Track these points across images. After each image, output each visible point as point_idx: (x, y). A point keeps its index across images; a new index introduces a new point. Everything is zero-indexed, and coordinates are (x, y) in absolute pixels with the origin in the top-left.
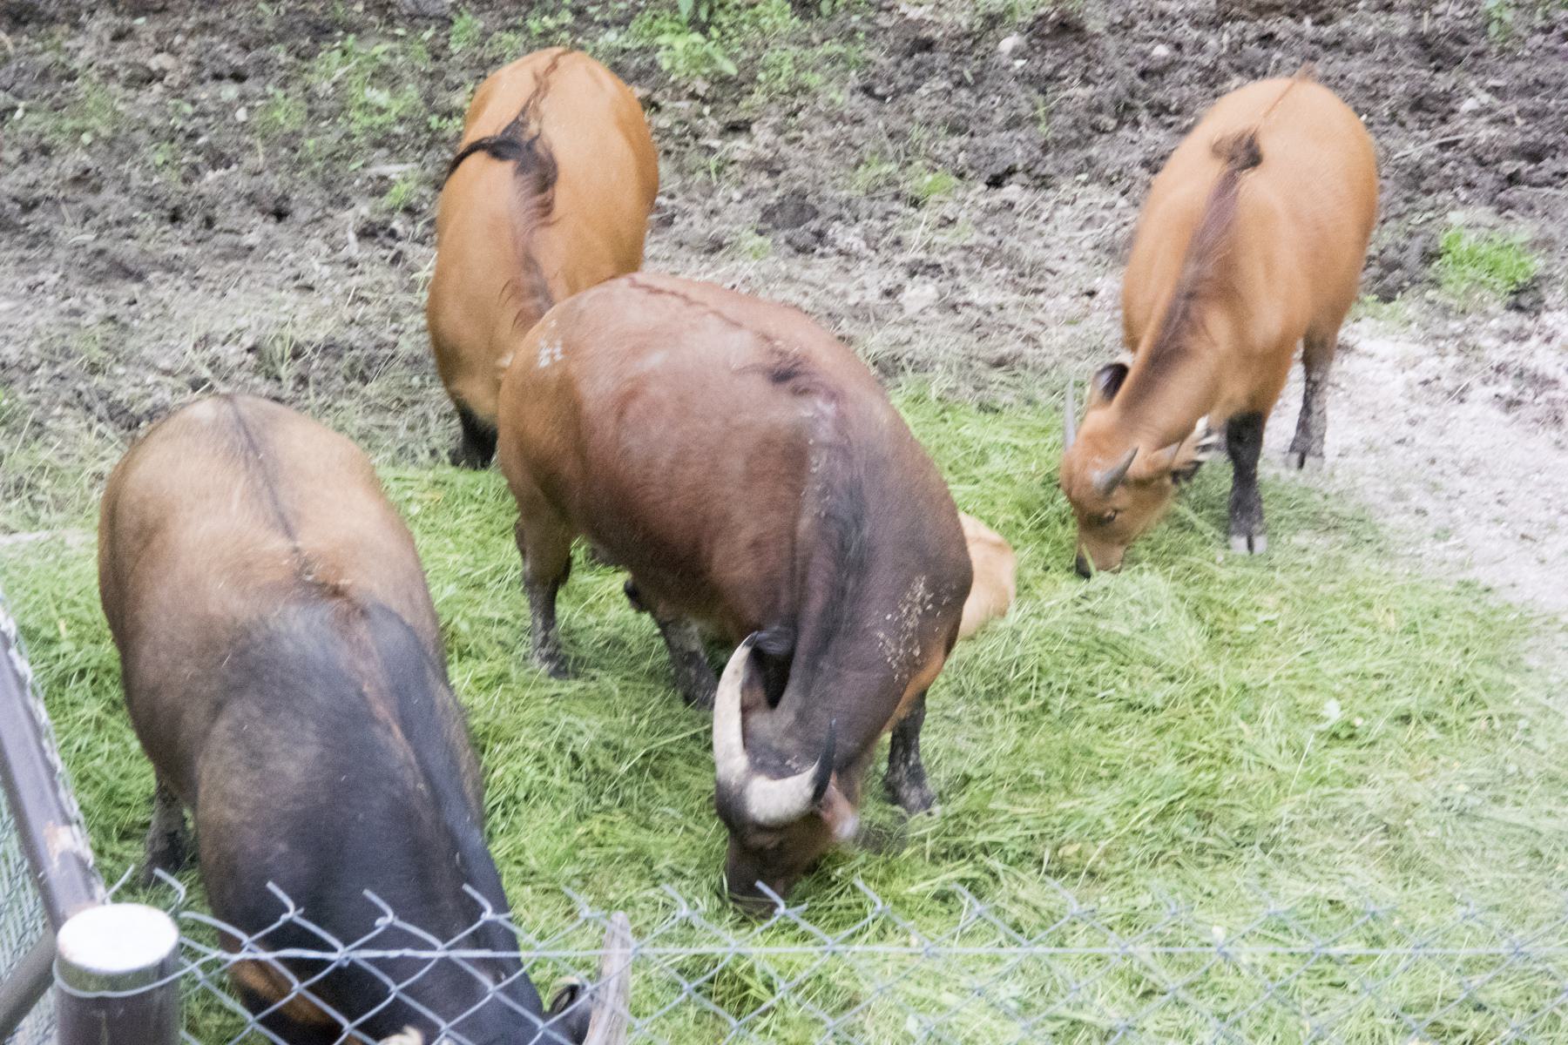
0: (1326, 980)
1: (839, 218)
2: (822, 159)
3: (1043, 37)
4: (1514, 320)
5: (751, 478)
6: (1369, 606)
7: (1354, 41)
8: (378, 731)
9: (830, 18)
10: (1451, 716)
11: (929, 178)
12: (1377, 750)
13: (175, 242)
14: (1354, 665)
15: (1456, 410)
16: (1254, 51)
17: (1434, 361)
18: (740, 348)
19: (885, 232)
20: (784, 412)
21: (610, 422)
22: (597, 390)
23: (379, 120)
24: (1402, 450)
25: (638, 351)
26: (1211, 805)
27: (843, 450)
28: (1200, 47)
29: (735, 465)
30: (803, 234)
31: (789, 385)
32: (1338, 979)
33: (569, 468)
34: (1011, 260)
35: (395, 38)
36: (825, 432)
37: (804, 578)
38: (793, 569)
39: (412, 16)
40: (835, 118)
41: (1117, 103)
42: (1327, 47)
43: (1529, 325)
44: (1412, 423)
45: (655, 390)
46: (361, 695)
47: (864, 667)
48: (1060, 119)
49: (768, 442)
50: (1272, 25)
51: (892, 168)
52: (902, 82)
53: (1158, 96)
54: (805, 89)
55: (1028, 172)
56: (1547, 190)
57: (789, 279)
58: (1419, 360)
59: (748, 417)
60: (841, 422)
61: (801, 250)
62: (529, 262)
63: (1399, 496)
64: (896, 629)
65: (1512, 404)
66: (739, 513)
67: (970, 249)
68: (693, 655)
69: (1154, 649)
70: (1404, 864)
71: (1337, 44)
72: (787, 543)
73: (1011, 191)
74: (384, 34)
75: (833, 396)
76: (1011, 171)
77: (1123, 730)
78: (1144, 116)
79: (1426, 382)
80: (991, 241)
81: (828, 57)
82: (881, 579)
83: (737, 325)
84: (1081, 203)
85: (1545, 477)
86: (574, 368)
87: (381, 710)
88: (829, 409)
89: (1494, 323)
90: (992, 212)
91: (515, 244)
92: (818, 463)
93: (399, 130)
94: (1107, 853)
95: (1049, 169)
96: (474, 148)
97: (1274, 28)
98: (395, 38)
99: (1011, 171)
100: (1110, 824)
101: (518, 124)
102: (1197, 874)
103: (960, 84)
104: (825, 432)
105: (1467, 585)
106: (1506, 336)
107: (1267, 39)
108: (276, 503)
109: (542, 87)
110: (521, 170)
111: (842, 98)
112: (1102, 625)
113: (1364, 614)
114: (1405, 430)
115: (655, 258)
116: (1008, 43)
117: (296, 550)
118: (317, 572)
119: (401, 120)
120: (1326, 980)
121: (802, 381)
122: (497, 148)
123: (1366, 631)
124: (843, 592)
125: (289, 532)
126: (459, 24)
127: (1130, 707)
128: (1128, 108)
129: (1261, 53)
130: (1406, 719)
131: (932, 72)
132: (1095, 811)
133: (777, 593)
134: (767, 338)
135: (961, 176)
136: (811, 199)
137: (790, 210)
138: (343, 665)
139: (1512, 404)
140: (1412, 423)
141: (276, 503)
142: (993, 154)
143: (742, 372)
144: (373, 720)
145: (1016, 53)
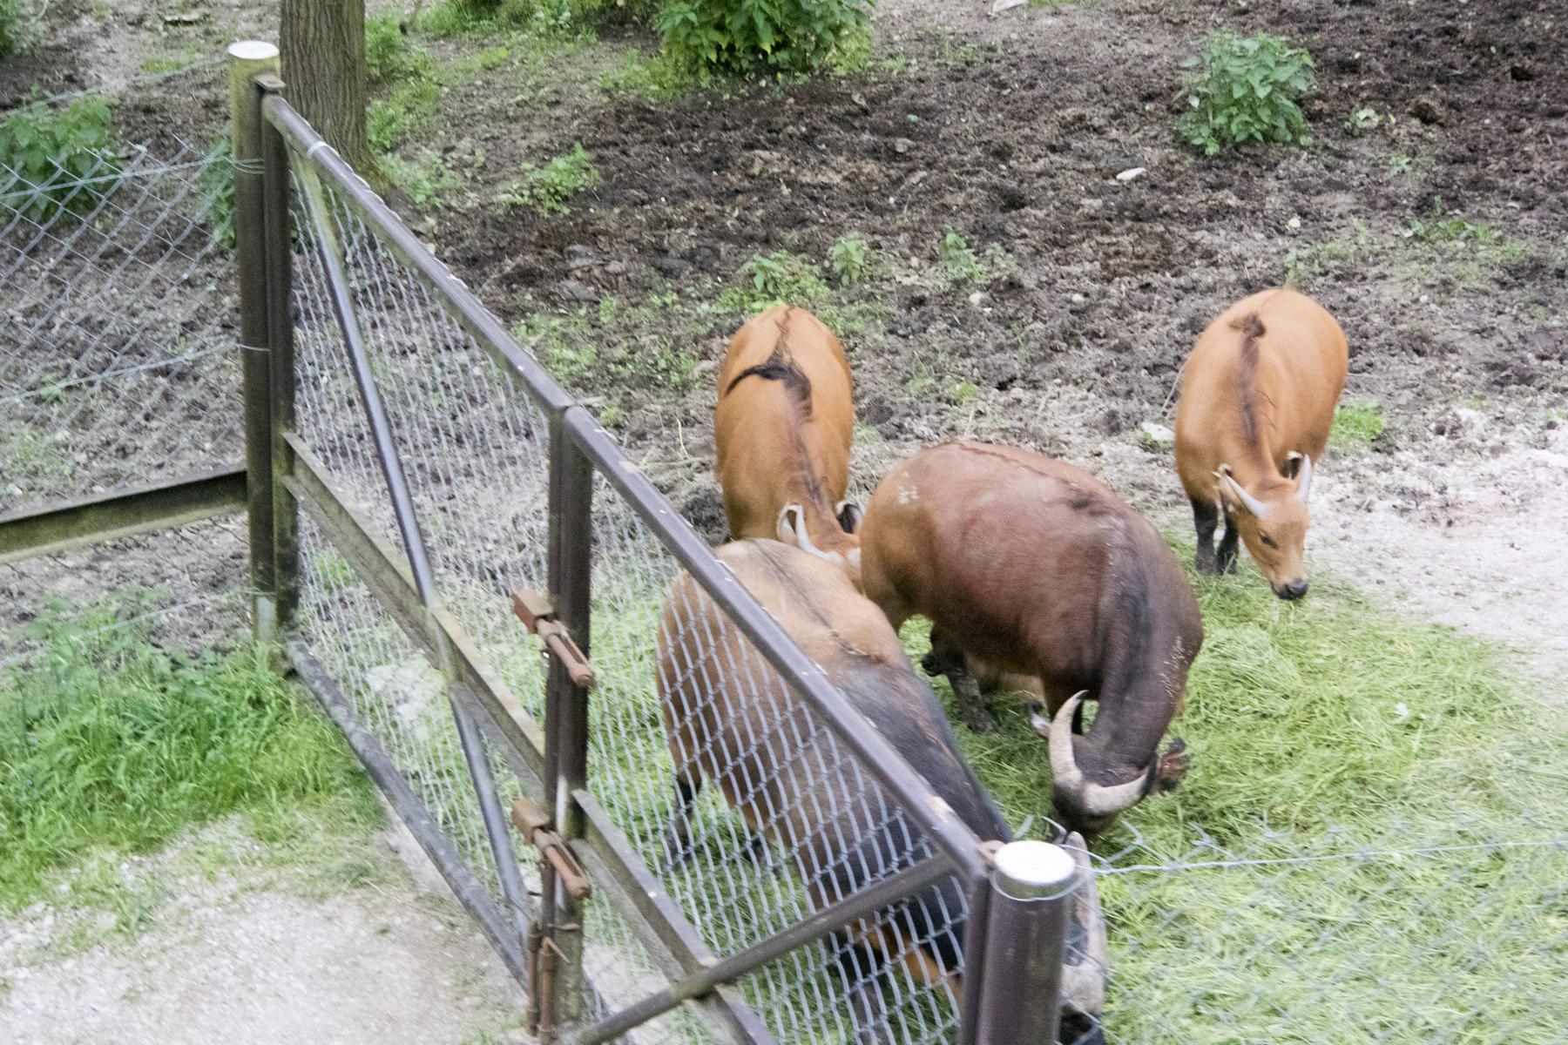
0: (1473, 884)
1: (908, 415)
2: (880, 377)
3: (999, 292)
4: (1380, 458)
5: (1062, 572)
6: (1391, 642)
7: (1202, 286)
8: (932, 750)
9: (849, 288)
10: (1482, 710)
11: (958, 387)
12: (1440, 734)
13: (463, 456)
14: (1401, 680)
15: (1368, 517)
16: (1139, 294)
17: (1340, 487)
18: (1047, 488)
19: (941, 422)
20: (1085, 527)
21: (956, 541)
22: (946, 519)
23: (574, 368)
24: (1346, 544)
25: (974, 493)
26: (1366, 774)
27: (1131, 550)
28: (1104, 294)
29: (1051, 563)
30: (887, 425)
31: (1088, 509)
32: (1481, 882)
33: (923, 572)
34: (1035, 436)
35: (561, 315)
36: (1118, 539)
37: (1106, 638)
38: (1095, 633)
39: (568, 300)
40: (879, 352)
41: (1064, 333)
42: (1186, 290)
43: (1390, 460)
44: (1344, 526)
45: (987, 518)
46: (917, 727)
47: (1155, 698)
48: (1032, 344)
49: (1074, 548)
50: (1147, 278)
51: (930, 381)
52: (916, 326)
53: (1089, 326)
54: (855, 333)
55: (1023, 378)
56: (1365, 375)
57: (893, 456)
58: (1331, 485)
59: (1059, 532)
60: (1129, 533)
61: (888, 438)
62: (800, 447)
63: (1361, 573)
64: (1169, 669)
65: (1404, 511)
66: (1053, 595)
67: (1006, 430)
68: (975, 698)
69: (1270, 678)
70: (1494, 802)
71: (1194, 288)
72: (1088, 615)
73: (1017, 391)
74: (552, 314)
75: (1120, 515)
76: (1012, 379)
77: (1263, 732)
78: (1084, 340)
79: (1341, 501)
80: (1020, 424)
81: (860, 313)
82: (1159, 637)
83: (1042, 474)
84: (1065, 397)
85: (1447, 556)
86: (928, 505)
87: (933, 735)
88: (1120, 523)
89: (1366, 460)
90: (1008, 406)
91: (790, 435)
92: (1115, 559)
93: (589, 374)
94: (1303, 810)
95: (1038, 376)
96: (747, 373)
97: (1150, 280)
98: (561, 315)
99: (1012, 379)
100: (1300, 791)
101: (776, 356)
102: (1366, 819)
103: (953, 325)
104: (1118, 539)
105: (1437, 626)
106: (1379, 469)
107: (1146, 287)
108: (809, 604)
109: (784, 329)
110: (789, 385)
111: (879, 337)
112: (1233, 663)
113: (1390, 648)
114: (1343, 532)
115: (862, 439)
116: (976, 297)
117: (836, 635)
118: (857, 649)
119: (589, 368)
120: (1473, 884)
121: (1097, 507)
122: (767, 372)
123: (1395, 658)
124: (1138, 647)
125: (826, 623)
126: (604, 304)
127: (1264, 716)
128: (1072, 335)
129: (1145, 296)
130: (1452, 713)
131: (933, 318)
132: (1288, 782)
133: (1080, 649)
134: (1066, 482)
135: (978, 384)
136: (887, 404)
137: (874, 411)
138: (900, 708)
139: (1404, 511)
140: (1344, 526)
141: (809, 604)
142: (999, 368)
143: (1050, 504)
144: (929, 743)
145: (984, 303)
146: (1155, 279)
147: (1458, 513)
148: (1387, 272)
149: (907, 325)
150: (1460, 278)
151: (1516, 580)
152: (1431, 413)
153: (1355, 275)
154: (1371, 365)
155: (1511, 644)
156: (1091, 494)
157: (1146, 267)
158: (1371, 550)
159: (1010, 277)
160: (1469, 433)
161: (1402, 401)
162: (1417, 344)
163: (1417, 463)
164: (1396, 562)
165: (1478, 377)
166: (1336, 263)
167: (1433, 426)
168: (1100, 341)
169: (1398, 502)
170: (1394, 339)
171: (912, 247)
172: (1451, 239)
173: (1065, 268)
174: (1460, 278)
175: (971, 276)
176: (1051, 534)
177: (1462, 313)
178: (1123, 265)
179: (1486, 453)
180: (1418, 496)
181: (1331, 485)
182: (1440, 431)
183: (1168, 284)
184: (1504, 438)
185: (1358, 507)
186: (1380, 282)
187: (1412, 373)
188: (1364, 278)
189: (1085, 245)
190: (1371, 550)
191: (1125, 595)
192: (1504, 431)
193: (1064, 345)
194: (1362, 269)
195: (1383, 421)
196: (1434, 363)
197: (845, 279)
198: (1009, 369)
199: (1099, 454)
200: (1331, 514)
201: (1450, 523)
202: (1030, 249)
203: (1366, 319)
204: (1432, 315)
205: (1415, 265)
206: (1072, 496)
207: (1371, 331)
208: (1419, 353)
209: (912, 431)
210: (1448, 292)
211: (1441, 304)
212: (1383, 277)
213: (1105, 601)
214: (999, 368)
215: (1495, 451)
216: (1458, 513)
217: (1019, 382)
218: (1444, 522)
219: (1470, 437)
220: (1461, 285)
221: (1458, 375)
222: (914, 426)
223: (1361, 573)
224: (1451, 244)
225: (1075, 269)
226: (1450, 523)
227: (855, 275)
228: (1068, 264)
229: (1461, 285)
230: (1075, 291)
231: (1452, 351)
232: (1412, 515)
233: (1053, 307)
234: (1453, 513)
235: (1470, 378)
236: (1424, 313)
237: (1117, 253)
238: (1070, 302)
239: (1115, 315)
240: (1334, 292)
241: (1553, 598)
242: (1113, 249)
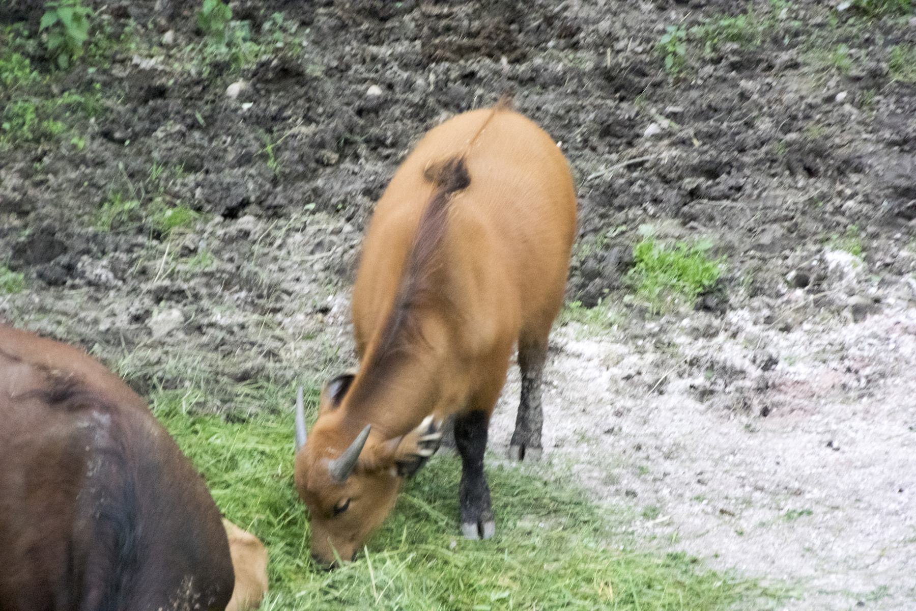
1: (87, 252)
2: (69, 199)
4: (703, 319)
5: (31, 488)
6: (589, 580)
11: (169, 213)
15: (656, 401)
17: (635, 358)
19: (131, 263)
24: (610, 439)
28: (409, 86)
30: (53, 268)
31: (66, 404)
34: (249, 283)
40: (77, 161)
41: (338, 139)
43: (716, 323)
44: (618, 414)
48: (286, 155)
50: (472, 65)
51: (133, 204)
53: (374, 131)
54: (48, 136)
55: (260, 203)
56: (725, 203)
58: (621, 357)
63: (611, 480)
67: (211, 275)
71: (532, 80)
73: (246, 221)
75: (106, 408)
78: (363, 150)
79: (628, 378)
80: (230, 267)
84: (311, 230)
85: (739, 457)
88: (105, 419)
89: (686, 322)
90: (228, 241)
92: (94, 468)
95: (280, 200)
97: (475, 67)
99: (245, 203)
104: (101, 439)
107: (469, 77)
113: (585, 588)
114: (612, 421)
121: (77, 400)
128: (348, 142)
129: (464, 90)
135: (199, 209)
136: (59, 236)
139: (705, 394)
140: (618, 414)
142: (228, 189)
143: (21, 398)
145: (243, 97)
146: (481, 65)
147: (779, 397)
148: (800, 59)
149: (127, 126)
150: (897, 68)
151: (816, 493)
152: (794, 257)
153: (760, 61)
154: (739, 189)
155: (764, 584)
156: (73, 383)
157: (477, 49)
158: (639, 448)
159: (283, 60)
160: (836, 285)
161: (766, 239)
162: (809, 160)
163: (750, 328)
164: (668, 466)
165: (876, 207)
166: (735, 46)
167: (792, 274)
168: (386, 152)
169: (700, 380)
170: (781, 154)
171: (172, 18)
172: (904, 13)
173: (374, 49)
174: (897, 68)
175: (235, 59)
176: (18, 440)
177: (885, 118)
178: (443, 46)
179: (846, 313)
180: (731, 373)
181: (621, 357)
182: (801, 282)
183: (497, 73)
184: (880, 293)
185: (650, 387)
186: (789, 72)
187: (790, 200)
188: (770, 67)
189: (407, 18)
190: (639, 448)
191: (105, 517)
192: (883, 283)
193: (334, 157)
194: (769, 53)
195: (720, 268)
196: (821, 186)
197: (63, 60)
198: (241, 190)
199: (325, 311)
200: (608, 396)
201: (765, 412)
202: (333, 22)
203: (749, 125)
204: (843, 121)
205: (843, 49)
206: (46, 387)
207: (750, 142)
208: (811, 172)
209: (82, 275)
210: (879, 87)
211: (860, 105)
212: (794, 65)
213: (81, 524)
214: (228, 189)
215: (859, 312)
216: (779, 397)
217: (253, 208)
218: (757, 409)
219: (837, 292)
220: (897, 77)
221: (850, 203)
222: (88, 269)
223: (611, 480)
224: (902, 20)
225: (384, 51)
226: (765, 412)
227: (79, 53)
228: (380, 43)
229: (897, 77)
230: (375, 82)
231: (858, 170)
232: (715, 399)
233: (336, 104)
234: (773, 397)
235: (866, 208)
236: (834, 117)
237: (448, 29)
238: (360, 95)
239: (414, 115)
240: (724, 86)
241: (850, 521)
242: (443, 23)
